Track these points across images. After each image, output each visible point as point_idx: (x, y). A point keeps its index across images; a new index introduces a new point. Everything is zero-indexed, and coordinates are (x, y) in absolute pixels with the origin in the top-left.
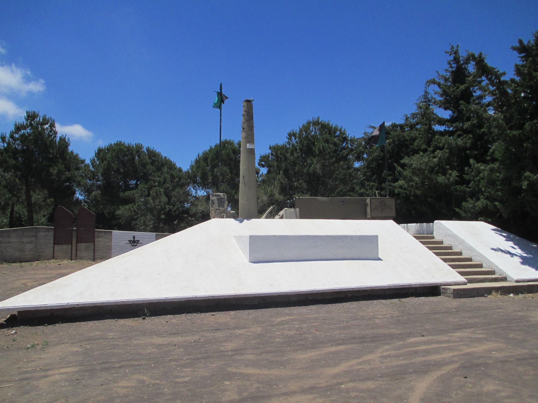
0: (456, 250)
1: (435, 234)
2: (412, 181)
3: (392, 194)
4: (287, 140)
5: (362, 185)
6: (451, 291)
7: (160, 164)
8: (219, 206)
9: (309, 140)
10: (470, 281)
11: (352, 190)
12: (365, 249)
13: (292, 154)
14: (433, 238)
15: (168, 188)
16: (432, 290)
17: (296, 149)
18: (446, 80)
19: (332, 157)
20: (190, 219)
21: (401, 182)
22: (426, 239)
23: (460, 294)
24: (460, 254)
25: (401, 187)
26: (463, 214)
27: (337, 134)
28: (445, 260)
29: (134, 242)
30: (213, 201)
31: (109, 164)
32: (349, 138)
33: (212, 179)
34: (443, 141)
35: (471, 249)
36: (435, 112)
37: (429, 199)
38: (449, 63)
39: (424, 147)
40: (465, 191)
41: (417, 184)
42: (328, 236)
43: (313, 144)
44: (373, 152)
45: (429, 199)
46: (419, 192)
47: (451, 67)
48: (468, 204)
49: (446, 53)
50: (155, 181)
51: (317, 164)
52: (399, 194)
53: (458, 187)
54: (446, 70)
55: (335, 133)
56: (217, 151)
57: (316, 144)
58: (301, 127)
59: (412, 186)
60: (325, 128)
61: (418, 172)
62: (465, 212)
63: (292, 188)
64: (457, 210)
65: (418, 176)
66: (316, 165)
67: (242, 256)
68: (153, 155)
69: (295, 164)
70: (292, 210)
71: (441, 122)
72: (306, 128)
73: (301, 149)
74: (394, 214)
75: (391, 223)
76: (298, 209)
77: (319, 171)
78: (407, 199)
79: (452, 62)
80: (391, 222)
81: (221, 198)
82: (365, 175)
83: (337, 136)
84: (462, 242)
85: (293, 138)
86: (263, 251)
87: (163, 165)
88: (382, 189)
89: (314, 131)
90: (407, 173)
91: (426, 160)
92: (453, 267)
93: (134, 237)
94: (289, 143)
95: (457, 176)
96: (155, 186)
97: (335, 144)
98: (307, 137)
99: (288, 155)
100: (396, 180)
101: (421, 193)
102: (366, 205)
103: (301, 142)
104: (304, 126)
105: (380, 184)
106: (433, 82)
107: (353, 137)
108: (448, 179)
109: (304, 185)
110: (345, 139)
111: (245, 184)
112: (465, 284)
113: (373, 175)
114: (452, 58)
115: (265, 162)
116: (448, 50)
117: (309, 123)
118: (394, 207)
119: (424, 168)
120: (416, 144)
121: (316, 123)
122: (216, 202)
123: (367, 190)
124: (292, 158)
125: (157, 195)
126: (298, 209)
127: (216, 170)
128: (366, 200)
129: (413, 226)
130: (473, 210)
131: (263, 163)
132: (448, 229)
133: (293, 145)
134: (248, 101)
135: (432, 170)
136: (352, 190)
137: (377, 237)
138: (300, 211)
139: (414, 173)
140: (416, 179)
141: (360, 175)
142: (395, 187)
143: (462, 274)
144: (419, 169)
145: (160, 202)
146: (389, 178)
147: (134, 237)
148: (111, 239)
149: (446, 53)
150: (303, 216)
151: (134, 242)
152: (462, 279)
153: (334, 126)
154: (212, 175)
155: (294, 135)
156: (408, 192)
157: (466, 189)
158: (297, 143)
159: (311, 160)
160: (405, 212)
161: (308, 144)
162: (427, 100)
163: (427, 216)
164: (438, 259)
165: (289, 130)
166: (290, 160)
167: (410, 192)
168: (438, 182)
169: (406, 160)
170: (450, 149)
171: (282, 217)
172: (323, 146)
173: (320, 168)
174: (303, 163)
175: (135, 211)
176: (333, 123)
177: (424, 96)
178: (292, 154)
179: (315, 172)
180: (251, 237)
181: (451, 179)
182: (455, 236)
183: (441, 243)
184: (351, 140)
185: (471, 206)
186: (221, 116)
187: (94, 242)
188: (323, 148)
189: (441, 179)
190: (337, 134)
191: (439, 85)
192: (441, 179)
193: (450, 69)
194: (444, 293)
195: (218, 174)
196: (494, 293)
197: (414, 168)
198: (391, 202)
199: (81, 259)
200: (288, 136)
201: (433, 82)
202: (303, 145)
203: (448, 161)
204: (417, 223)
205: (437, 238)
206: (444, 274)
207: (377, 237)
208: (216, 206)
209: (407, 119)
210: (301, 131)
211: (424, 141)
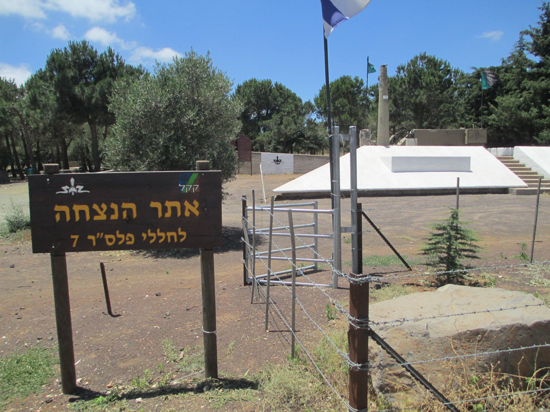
0: (527, 167)
1: (514, 156)
2: (503, 115)
3: (486, 125)
4: (396, 73)
5: (462, 116)
6: (515, 191)
7: (286, 96)
8: (366, 138)
9: (416, 74)
10: (529, 186)
11: (455, 121)
12: (463, 165)
13: (401, 86)
14: (513, 158)
15: (295, 116)
16: (504, 191)
17: (404, 82)
18: (537, 31)
19: (436, 89)
20: (305, 141)
21: (493, 116)
22: (507, 161)
23: (521, 192)
24: (530, 169)
25: (494, 120)
26: (539, 141)
27: (442, 68)
28: (516, 174)
29: (277, 161)
30: (362, 134)
31: (249, 99)
32: (453, 70)
33: (333, 110)
34: (529, 84)
35: (537, 166)
36: (527, 57)
37: (515, 129)
38: (541, 17)
39: (515, 87)
40: (543, 124)
41: (506, 118)
42: (439, 157)
43: (420, 76)
44: (473, 91)
45: (515, 129)
46: (508, 124)
47: (543, 20)
48: (544, 133)
49: (539, 8)
50: (284, 111)
51: (423, 95)
52: (492, 125)
53: (538, 121)
54: (539, 23)
55: (440, 66)
56: (338, 85)
57: (422, 77)
58: (409, 62)
59: (502, 119)
60: (433, 63)
61: (506, 109)
62: (542, 140)
63: (399, 115)
64: (535, 138)
65: (506, 112)
66: (422, 97)
67: (387, 169)
68: (279, 88)
69: (402, 94)
70: (412, 139)
71: (531, 65)
72: (414, 62)
73: (409, 82)
74: (485, 141)
75: (481, 149)
76: (416, 139)
77: (424, 101)
78: (498, 128)
79: (543, 16)
80: (482, 148)
81: (367, 133)
82: (466, 109)
83: (442, 69)
84: (532, 161)
85: (402, 71)
86: (400, 165)
87: (289, 97)
88: (479, 121)
89: (421, 64)
90: (498, 110)
91: (513, 99)
92: (521, 178)
93: (277, 157)
94: (398, 76)
95: (537, 112)
96: (285, 116)
97: (440, 77)
98: (414, 71)
99: (397, 87)
100: (490, 114)
101: (509, 125)
102: (464, 135)
103: (409, 75)
104: (412, 61)
105: (477, 116)
106: (527, 33)
107: (456, 68)
108: (530, 115)
109: (411, 113)
110: (449, 71)
111: (382, 122)
112: (526, 187)
113: (472, 108)
114: (544, 12)
115: (375, 92)
116: (541, 6)
117: (416, 58)
118: (486, 136)
119: (512, 106)
120: (508, 85)
121: (423, 57)
122: (364, 135)
123: (466, 121)
124: (400, 89)
125: (289, 123)
126: (416, 139)
127: (336, 102)
128: (464, 130)
129: (501, 150)
130: (547, 138)
131: (373, 93)
132: (526, 153)
133: (402, 79)
134: (384, 66)
135: (519, 107)
136: (455, 121)
137: (469, 158)
138: (418, 140)
139: (503, 110)
140: (506, 114)
141: (462, 109)
142: (489, 119)
143: (526, 182)
144: (508, 107)
145: (291, 129)
146: (485, 112)
147: (277, 157)
148: (260, 159)
149: (539, 8)
150: (420, 144)
151: (277, 161)
152: (526, 185)
153: (439, 60)
154: (334, 106)
155: (403, 68)
156: (499, 124)
157: (543, 122)
158: (405, 75)
159: (419, 91)
160: (496, 138)
161: (415, 77)
162: (522, 46)
163: (510, 143)
164: (511, 172)
165: (399, 64)
166: (399, 91)
167: (501, 124)
168: (522, 117)
169: (498, 99)
170: (535, 89)
171: (404, 144)
172: (430, 80)
173: (426, 99)
174: (410, 93)
175: (271, 137)
176: (439, 57)
177: (519, 41)
178: (401, 86)
179: (421, 103)
180: (393, 157)
181: (532, 115)
182: (528, 158)
183: (518, 162)
184: (454, 72)
185: (546, 135)
186: (535, 227)
187: (251, 161)
188: (430, 83)
189: (524, 114)
190: (442, 68)
191: (532, 35)
192: (524, 114)
193: (542, 22)
194: (511, 192)
195: (339, 106)
196: (544, 193)
197: (504, 107)
198: (484, 132)
199: (255, 174)
200: (397, 70)
201: (527, 33)
202: (410, 78)
203: (533, 100)
204: (504, 147)
205: (516, 159)
206: (513, 180)
207: (469, 158)
208: (364, 138)
209: (503, 62)
210: (409, 65)
211: (515, 83)
